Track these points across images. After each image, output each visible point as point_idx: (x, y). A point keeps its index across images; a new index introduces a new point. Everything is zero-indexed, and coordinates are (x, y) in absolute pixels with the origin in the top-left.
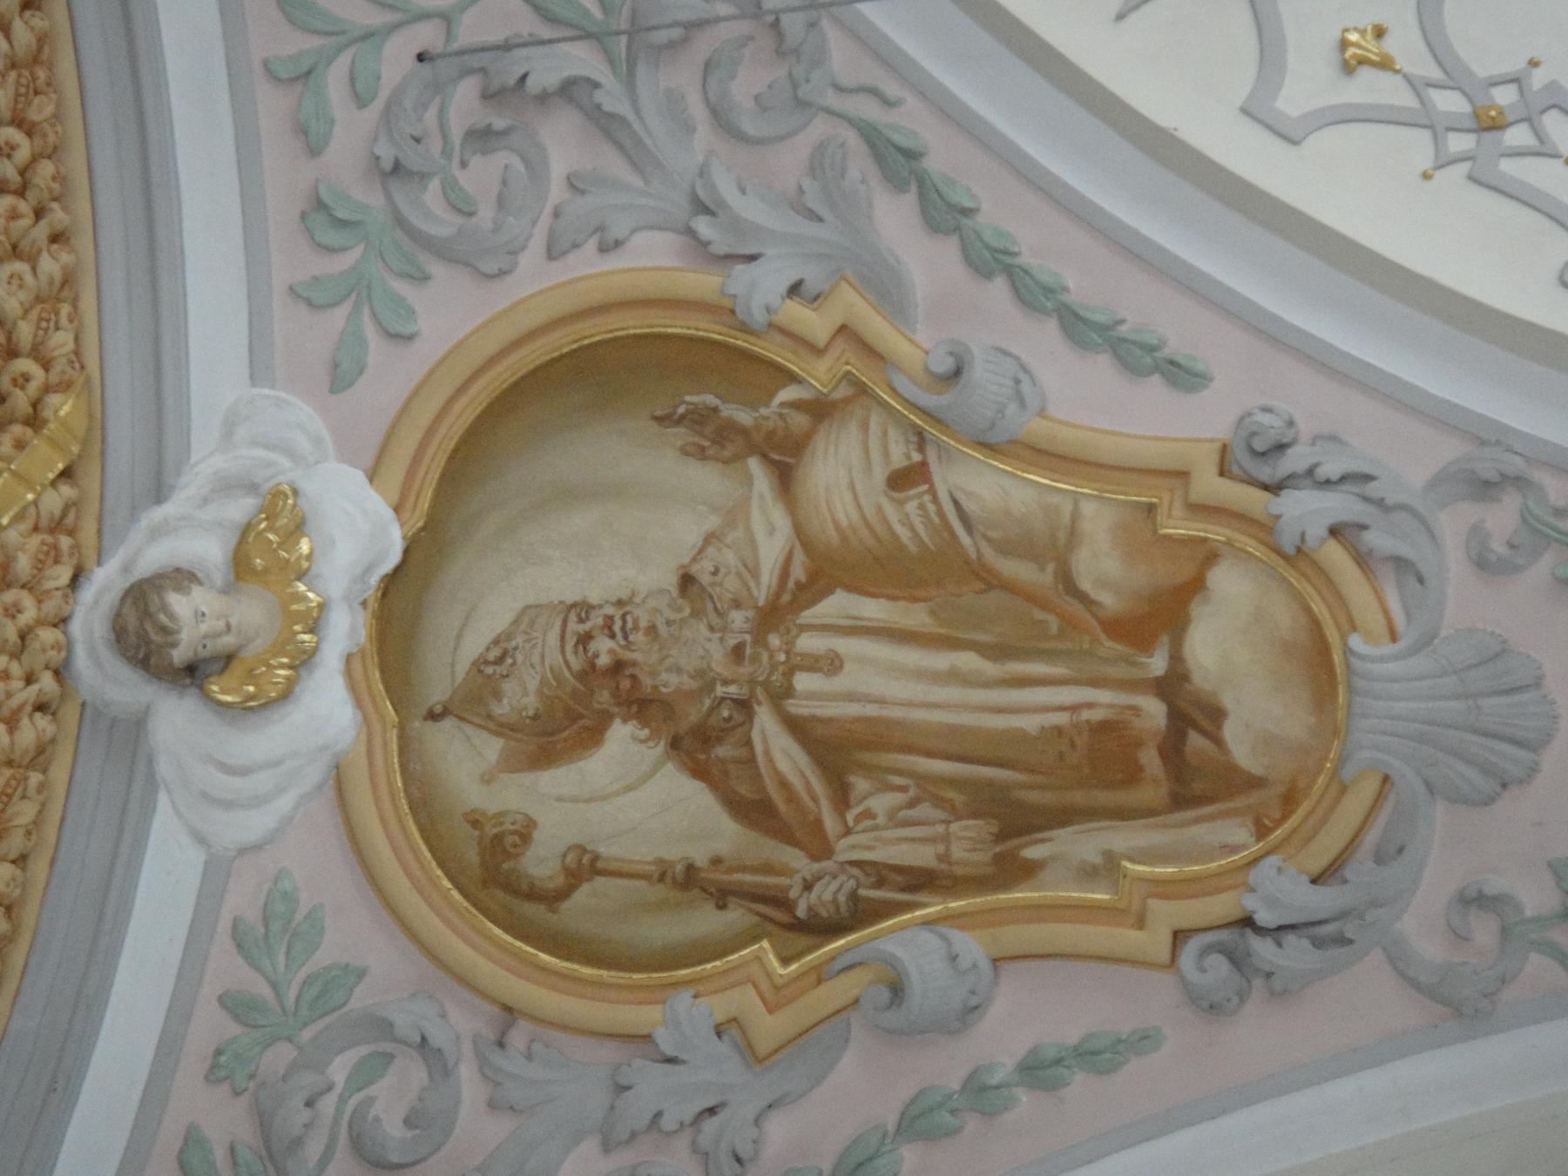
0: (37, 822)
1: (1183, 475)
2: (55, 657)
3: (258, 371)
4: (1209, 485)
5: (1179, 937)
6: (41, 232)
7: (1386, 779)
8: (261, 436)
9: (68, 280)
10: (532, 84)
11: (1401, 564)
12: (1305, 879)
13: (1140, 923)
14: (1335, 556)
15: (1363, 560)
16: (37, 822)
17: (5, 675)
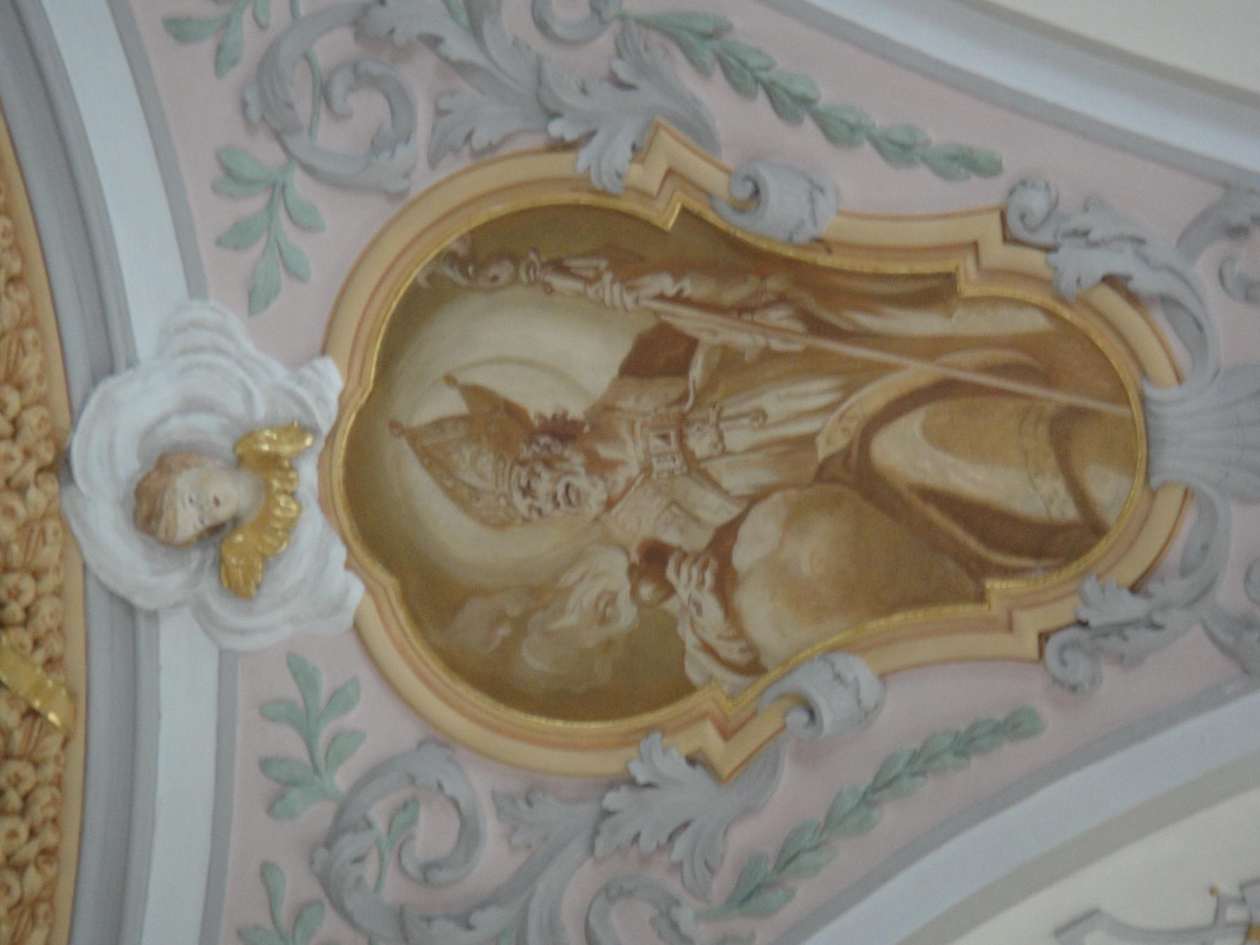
0: (45, 366)
1: (975, 246)
2: (51, 812)
3: (196, 286)
4: (997, 253)
5: (1044, 637)
6: (31, 850)
7: (1186, 492)
8: (206, 342)
9: (48, 895)
10: (399, 38)
11: (1166, 301)
12: (1125, 593)
13: (1010, 627)
14: (1111, 301)
15: (1133, 299)
16: (45, 366)
17: (9, 458)
